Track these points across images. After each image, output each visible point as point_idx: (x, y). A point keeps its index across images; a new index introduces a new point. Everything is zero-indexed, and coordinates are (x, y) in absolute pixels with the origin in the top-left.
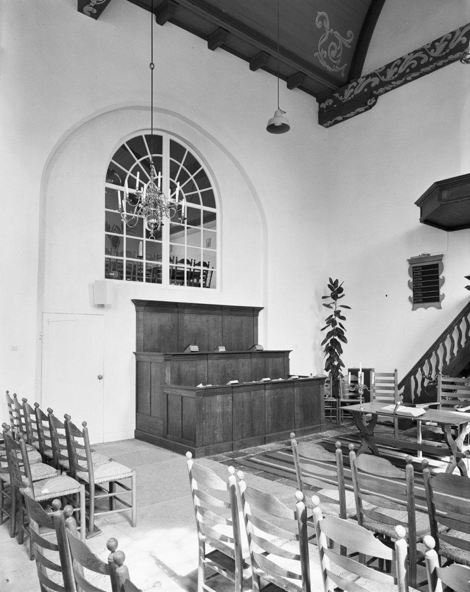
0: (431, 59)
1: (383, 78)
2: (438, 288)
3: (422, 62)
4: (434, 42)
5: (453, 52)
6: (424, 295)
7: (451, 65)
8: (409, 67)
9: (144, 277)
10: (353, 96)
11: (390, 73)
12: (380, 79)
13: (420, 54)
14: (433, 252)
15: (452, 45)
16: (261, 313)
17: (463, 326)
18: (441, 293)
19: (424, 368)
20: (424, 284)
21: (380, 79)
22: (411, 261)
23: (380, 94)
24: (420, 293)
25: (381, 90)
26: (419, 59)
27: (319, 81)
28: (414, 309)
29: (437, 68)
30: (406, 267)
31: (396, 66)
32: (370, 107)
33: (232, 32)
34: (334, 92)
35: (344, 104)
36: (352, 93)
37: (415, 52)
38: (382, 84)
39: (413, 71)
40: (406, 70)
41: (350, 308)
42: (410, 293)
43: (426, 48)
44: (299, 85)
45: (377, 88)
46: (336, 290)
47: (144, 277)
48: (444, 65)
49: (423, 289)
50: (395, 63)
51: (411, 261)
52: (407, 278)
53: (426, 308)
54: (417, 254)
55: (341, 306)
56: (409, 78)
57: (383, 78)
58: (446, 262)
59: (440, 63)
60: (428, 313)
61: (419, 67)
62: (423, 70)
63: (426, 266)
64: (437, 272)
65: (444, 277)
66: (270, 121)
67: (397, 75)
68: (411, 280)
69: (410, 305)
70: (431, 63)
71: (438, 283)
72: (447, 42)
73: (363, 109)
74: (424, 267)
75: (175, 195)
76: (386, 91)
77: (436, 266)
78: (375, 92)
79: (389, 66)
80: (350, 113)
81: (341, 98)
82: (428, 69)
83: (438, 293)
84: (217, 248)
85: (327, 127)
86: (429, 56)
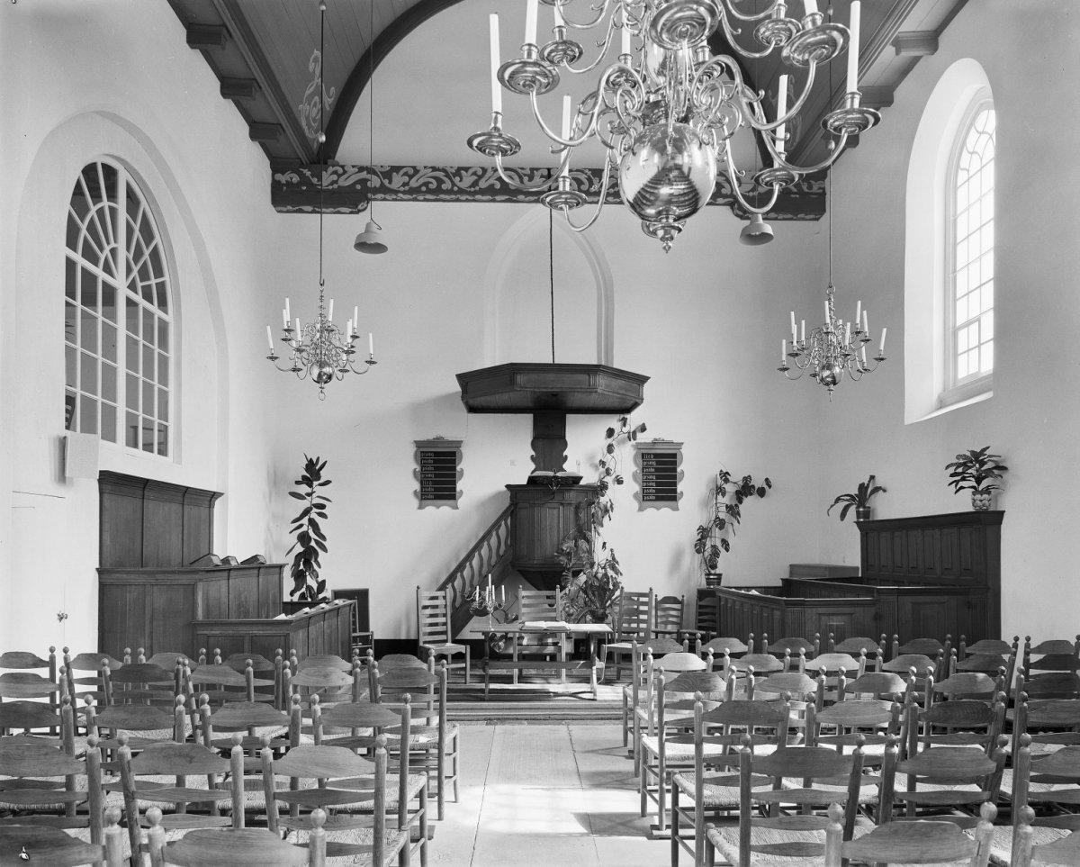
0: (456, 189)
1: (386, 182)
2: (454, 483)
3: (444, 187)
4: (460, 169)
5: (482, 192)
6: (436, 489)
7: (473, 203)
8: (426, 184)
9: (156, 448)
10: (335, 186)
11: (398, 181)
12: (381, 182)
13: (440, 174)
14: (450, 434)
15: (483, 184)
16: (218, 503)
17: (503, 531)
18: (458, 489)
19: (456, 584)
20: (436, 476)
21: (381, 182)
22: (419, 444)
23: (376, 200)
24: (430, 487)
25: (379, 196)
26: (440, 181)
27: (294, 144)
28: (421, 507)
29: (458, 200)
30: (411, 450)
31: (406, 174)
32: (359, 211)
33: (236, 39)
34: (302, 165)
35: (319, 191)
36: (336, 182)
37: (434, 169)
38: (384, 190)
39: (429, 191)
40: (420, 186)
41: (62, 476)
42: (416, 486)
43: (449, 170)
44: (263, 140)
45: (375, 191)
46: (313, 472)
47: (156, 448)
48: (467, 200)
49: (435, 483)
50: (405, 170)
51: (419, 444)
52: (414, 466)
53: (438, 507)
54: (428, 435)
55: (318, 497)
56: (421, 198)
57: (386, 182)
58: (464, 449)
59: (464, 198)
60: (439, 513)
61: (438, 191)
62: (442, 196)
63: (439, 452)
64: (454, 462)
65: (462, 470)
66: (359, 236)
67: (407, 188)
68: (418, 469)
69: (416, 502)
70: (456, 193)
71: (454, 476)
72: (476, 178)
73: (348, 210)
74: (436, 454)
75: (136, 293)
76: (385, 199)
77: (674, 456)
78: (369, 195)
79: (396, 169)
80: (327, 208)
81: (315, 180)
82: (447, 197)
83: (454, 489)
84: (170, 386)
85: (278, 212)
86: (454, 184)
